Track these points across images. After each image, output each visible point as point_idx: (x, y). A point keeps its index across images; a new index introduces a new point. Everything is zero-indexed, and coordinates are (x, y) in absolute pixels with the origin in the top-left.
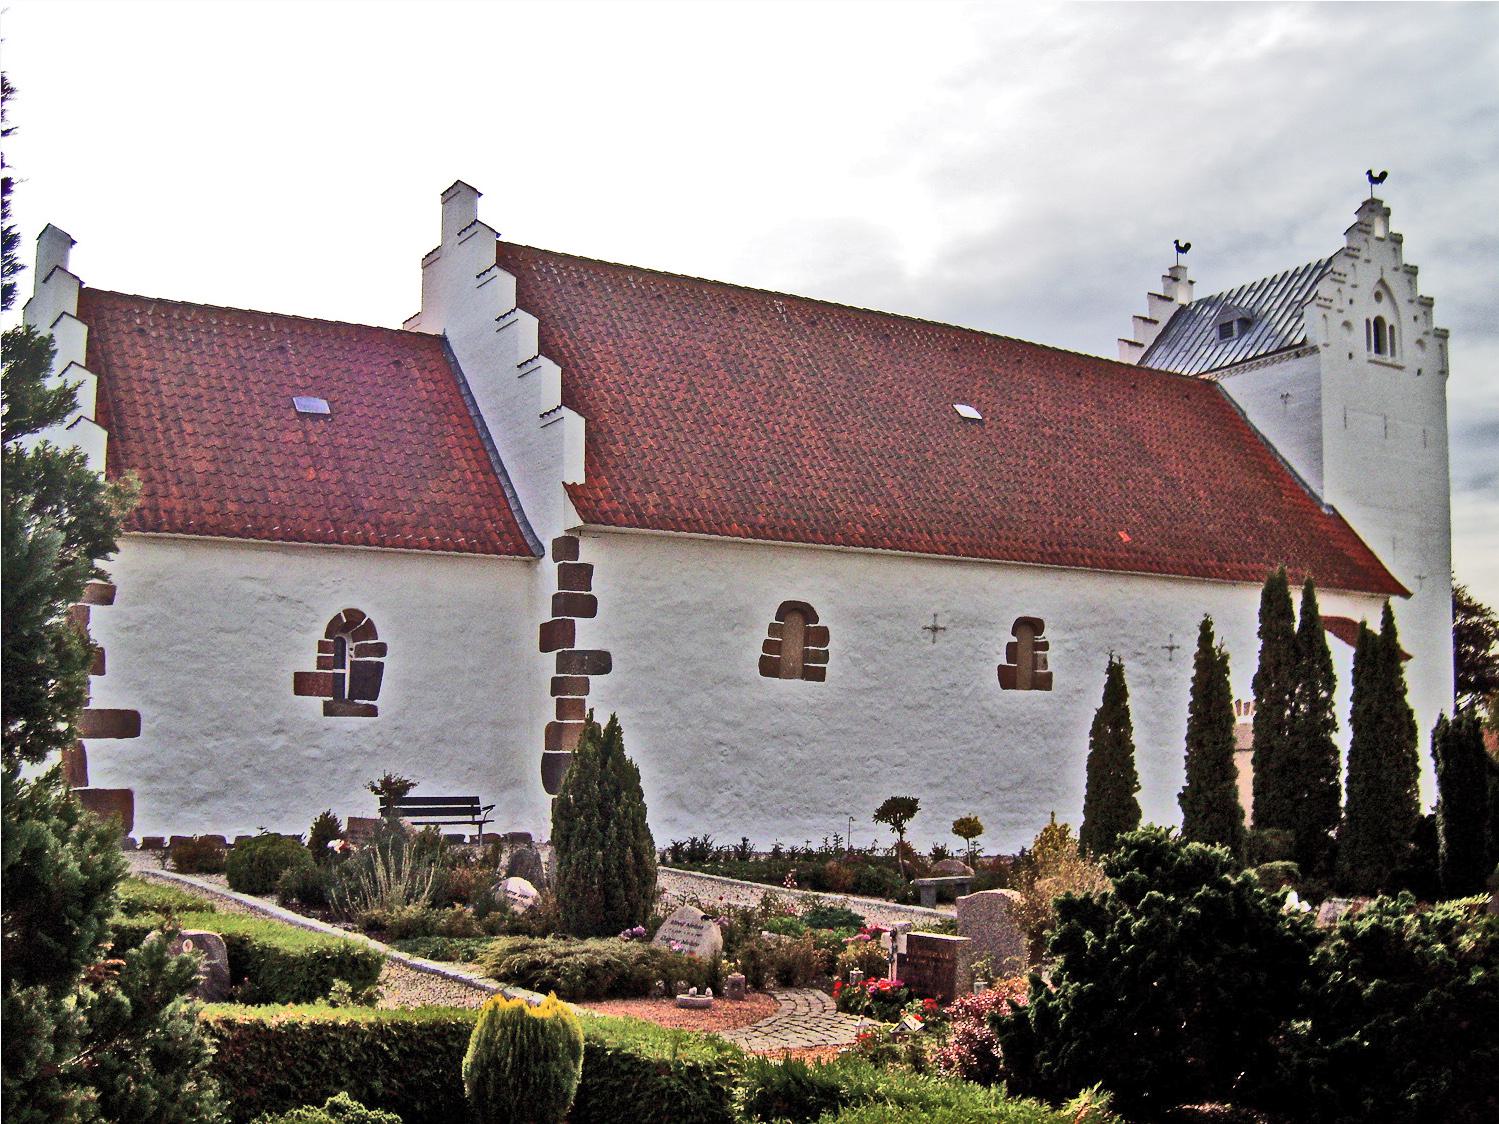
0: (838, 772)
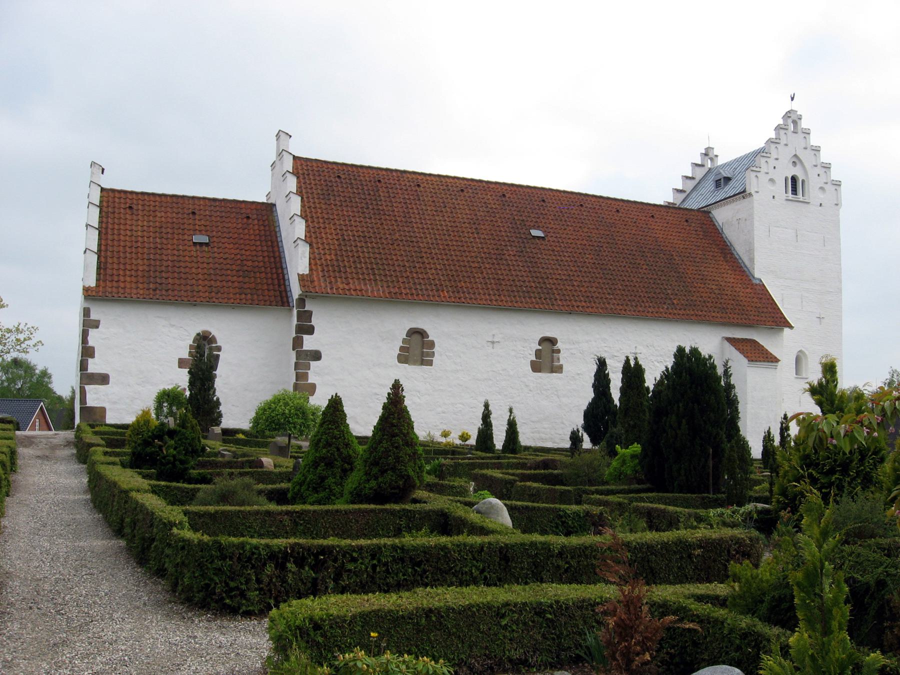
0: (440, 410)
